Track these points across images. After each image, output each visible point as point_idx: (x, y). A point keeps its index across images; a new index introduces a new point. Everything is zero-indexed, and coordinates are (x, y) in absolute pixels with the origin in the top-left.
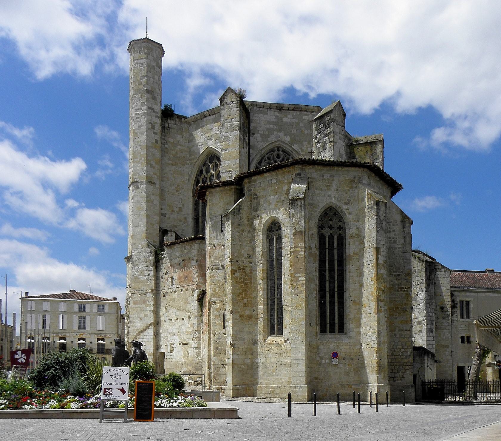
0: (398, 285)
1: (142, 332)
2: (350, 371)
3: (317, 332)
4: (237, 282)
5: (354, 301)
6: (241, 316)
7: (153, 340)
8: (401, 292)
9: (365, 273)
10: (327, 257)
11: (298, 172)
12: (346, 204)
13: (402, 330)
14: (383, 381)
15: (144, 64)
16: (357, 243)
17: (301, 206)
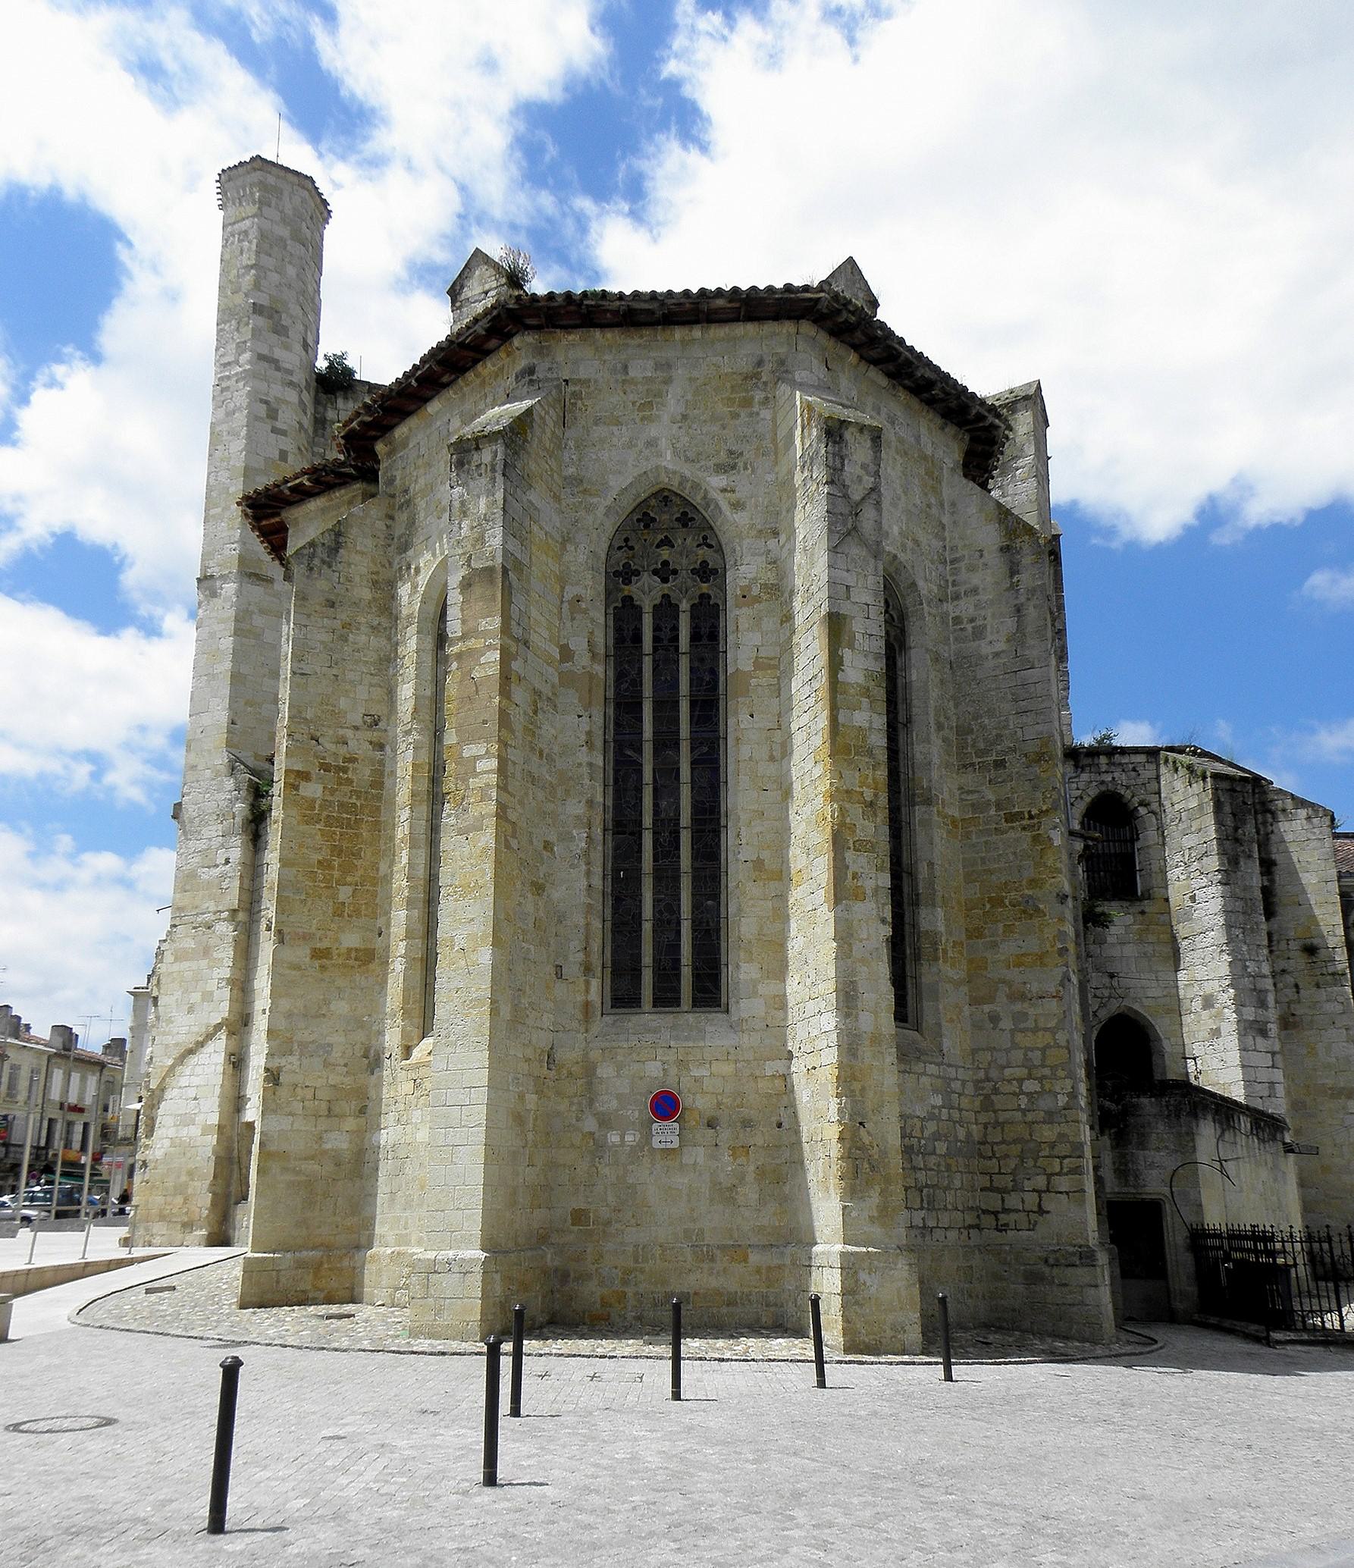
0: (999, 806)
1: (191, 1052)
2: (742, 1179)
3: (587, 1005)
4: (310, 820)
5: (759, 864)
6: (318, 954)
7: (219, 1080)
8: (1012, 834)
9: (798, 738)
10: (647, 690)
11: (522, 364)
12: (721, 469)
13: (1023, 997)
14: (877, 1231)
15: (251, 232)
16: (769, 623)
17: (493, 470)
